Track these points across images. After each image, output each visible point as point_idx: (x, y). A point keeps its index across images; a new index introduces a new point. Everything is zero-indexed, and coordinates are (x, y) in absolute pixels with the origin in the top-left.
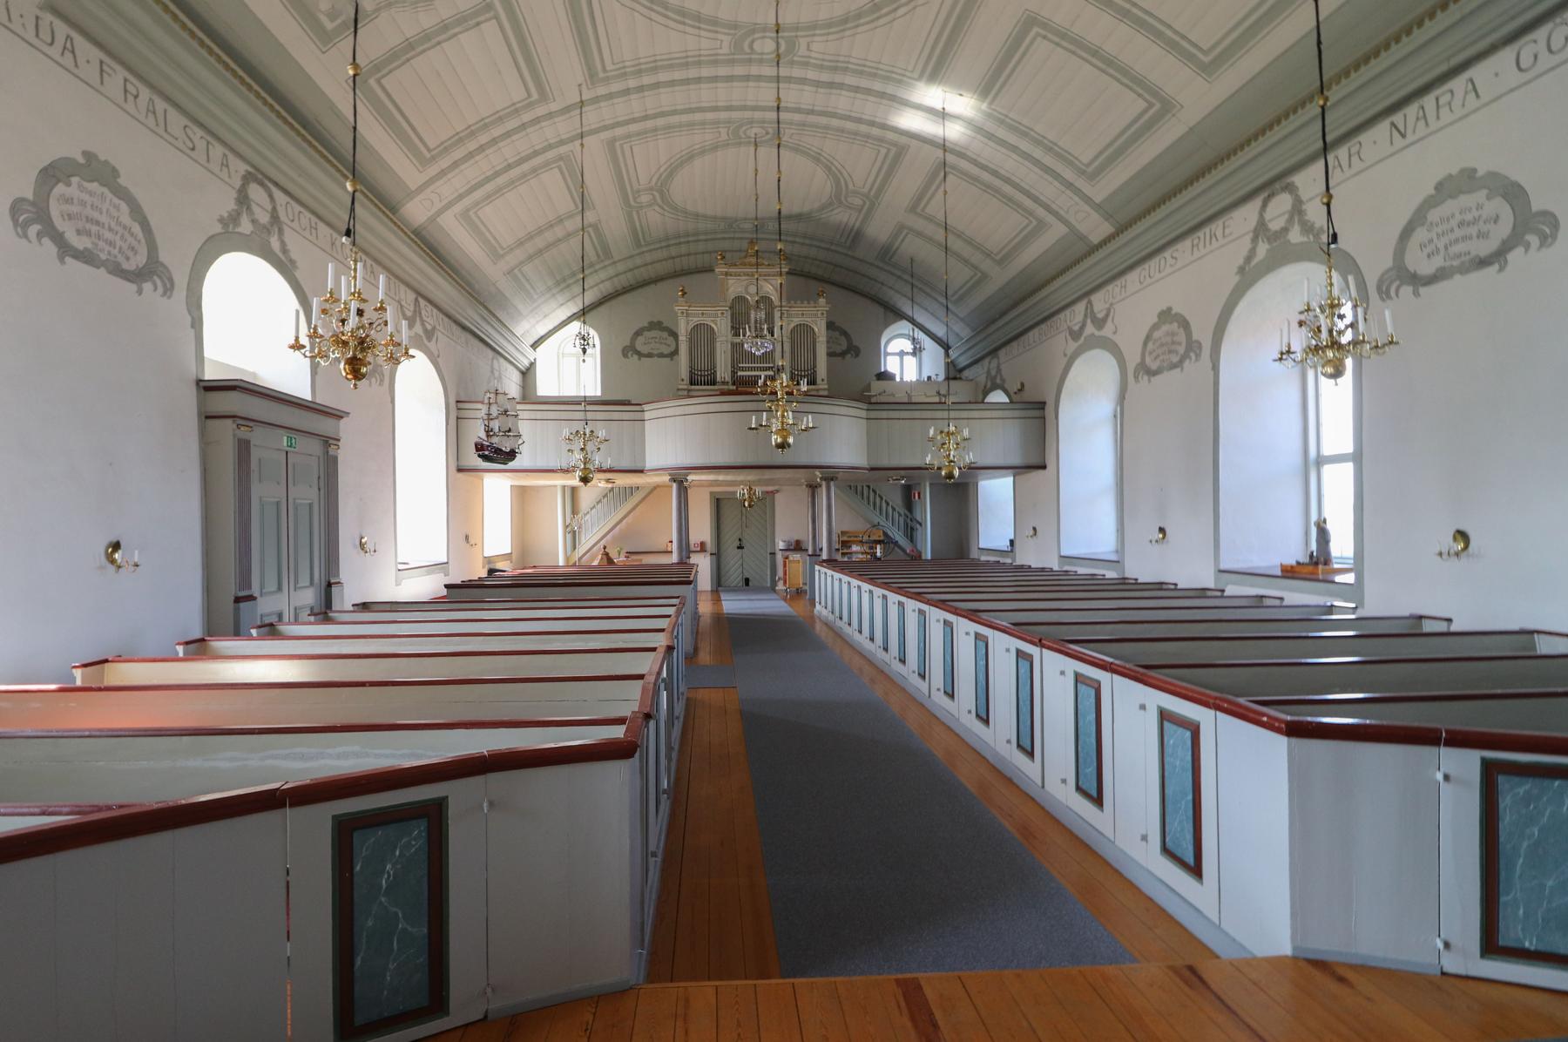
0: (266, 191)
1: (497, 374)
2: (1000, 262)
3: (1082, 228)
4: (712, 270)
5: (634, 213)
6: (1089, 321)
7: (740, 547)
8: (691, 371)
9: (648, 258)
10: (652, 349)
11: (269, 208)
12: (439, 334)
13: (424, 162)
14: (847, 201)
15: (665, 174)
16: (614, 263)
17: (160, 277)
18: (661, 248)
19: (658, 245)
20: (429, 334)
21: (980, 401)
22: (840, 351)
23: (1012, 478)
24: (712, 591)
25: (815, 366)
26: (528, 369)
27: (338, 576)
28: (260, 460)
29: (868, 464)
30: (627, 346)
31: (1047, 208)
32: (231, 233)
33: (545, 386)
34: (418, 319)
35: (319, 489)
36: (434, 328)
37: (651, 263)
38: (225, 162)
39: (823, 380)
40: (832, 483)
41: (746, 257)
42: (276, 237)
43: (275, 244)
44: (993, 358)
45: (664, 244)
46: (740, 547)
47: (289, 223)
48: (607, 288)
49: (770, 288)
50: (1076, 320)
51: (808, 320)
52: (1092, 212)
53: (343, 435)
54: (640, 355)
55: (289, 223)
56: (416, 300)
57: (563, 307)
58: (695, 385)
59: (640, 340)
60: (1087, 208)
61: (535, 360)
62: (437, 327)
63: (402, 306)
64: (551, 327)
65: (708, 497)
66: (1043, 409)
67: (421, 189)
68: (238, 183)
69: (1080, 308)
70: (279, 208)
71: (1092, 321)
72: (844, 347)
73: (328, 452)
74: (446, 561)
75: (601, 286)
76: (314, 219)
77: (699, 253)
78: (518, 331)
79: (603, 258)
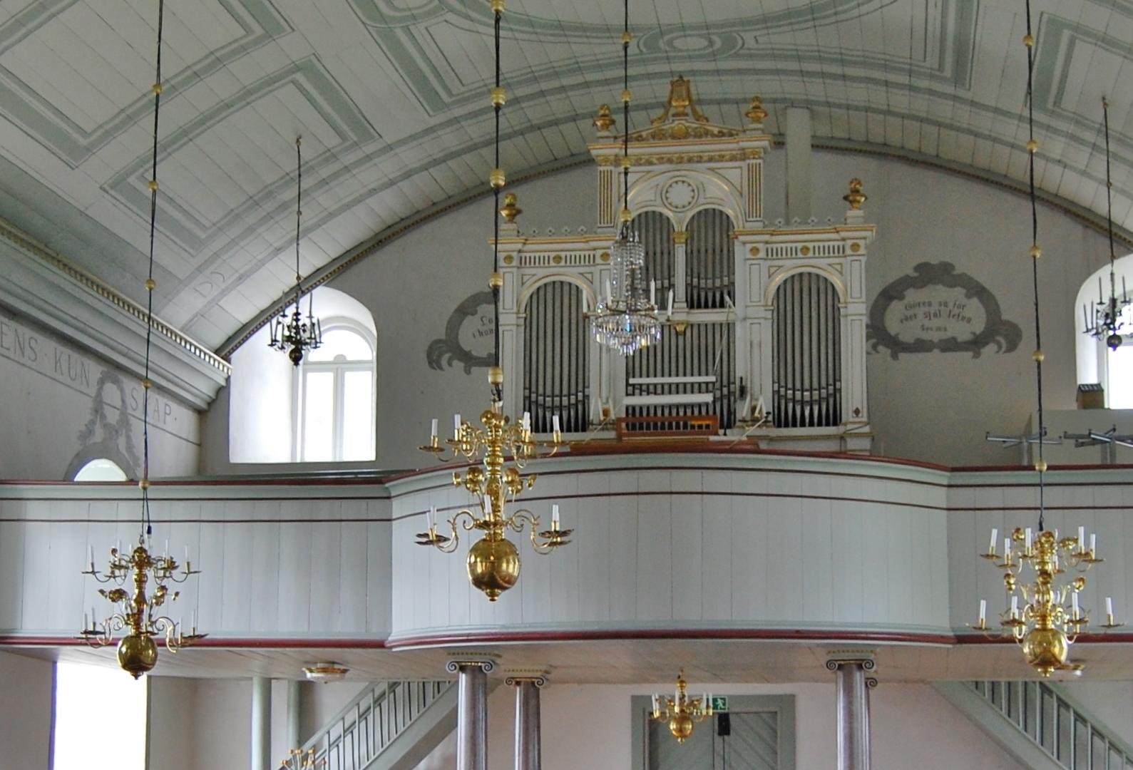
1: (113, 417)
5: (400, 34)
14: (396, 9)
16: (390, 147)
26: (211, 403)
30: (439, 341)
39: (857, 412)
41: (663, 119)
48: (387, 206)
51: (822, 266)
58: (786, 425)
59: (895, 311)
61: (228, 379)
65: (626, 706)
72: (979, 326)
75: (371, 201)
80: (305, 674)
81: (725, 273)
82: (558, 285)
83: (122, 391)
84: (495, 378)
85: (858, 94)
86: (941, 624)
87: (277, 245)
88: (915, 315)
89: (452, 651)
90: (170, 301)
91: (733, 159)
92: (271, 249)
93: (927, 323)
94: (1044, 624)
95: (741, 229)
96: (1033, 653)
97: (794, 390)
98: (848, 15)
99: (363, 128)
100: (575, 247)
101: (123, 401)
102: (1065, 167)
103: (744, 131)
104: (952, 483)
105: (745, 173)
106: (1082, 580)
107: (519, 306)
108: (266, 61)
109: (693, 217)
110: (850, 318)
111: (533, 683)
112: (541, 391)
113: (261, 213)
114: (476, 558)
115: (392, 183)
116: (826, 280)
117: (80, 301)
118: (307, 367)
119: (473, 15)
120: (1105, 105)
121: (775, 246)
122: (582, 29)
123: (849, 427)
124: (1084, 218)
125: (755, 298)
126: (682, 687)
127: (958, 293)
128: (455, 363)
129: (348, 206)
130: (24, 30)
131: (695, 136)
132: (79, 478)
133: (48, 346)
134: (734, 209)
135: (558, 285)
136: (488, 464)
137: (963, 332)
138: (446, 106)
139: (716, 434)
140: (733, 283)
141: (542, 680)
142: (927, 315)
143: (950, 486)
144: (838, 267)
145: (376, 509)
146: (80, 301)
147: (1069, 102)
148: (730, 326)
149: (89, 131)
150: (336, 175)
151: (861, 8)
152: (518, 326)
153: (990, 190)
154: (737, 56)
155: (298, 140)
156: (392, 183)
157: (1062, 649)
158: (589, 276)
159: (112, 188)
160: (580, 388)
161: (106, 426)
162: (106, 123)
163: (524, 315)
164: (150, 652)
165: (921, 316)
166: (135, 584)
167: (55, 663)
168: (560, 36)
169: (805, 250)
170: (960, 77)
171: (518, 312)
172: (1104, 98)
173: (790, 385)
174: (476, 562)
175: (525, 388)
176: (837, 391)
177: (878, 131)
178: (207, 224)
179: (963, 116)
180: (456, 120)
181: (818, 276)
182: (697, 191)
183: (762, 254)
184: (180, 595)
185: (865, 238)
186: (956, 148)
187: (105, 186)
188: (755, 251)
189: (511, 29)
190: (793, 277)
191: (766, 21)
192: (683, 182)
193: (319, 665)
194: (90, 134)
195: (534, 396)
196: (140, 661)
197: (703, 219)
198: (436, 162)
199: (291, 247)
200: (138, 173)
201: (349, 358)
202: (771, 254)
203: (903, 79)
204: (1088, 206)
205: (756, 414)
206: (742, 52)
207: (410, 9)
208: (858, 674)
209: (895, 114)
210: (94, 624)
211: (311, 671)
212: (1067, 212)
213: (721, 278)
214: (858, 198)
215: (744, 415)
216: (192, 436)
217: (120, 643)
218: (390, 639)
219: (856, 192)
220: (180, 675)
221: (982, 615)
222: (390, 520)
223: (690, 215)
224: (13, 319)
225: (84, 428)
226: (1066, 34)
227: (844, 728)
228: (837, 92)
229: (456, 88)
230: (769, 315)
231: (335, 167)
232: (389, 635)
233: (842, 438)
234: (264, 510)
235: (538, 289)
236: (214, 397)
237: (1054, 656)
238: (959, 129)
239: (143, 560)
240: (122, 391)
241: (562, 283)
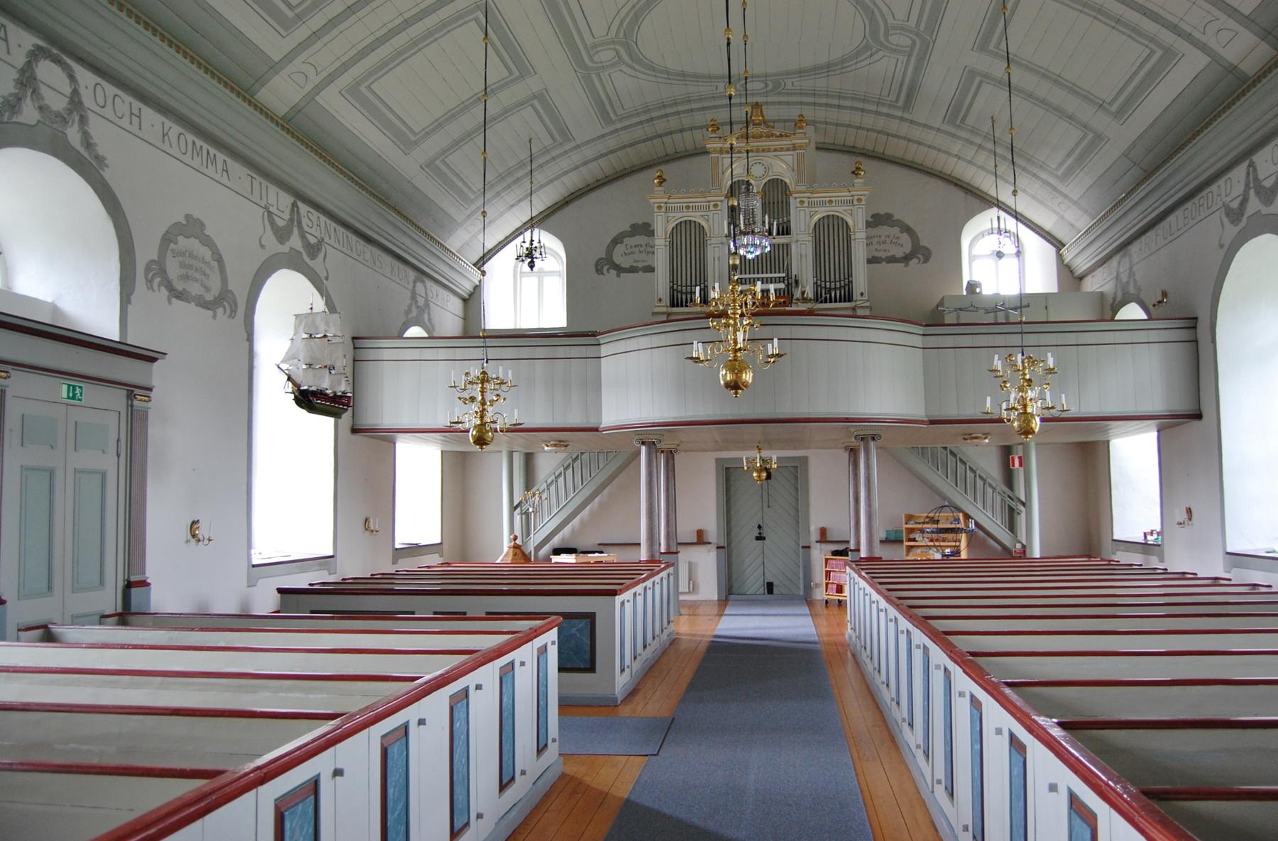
0: (63, 70)
1: (421, 302)
2: (1119, 114)
3: (1231, 54)
4: (705, 152)
6: (1252, 192)
7: (760, 538)
8: (672, 288)
9: (626, 137)
10: (635, 261)
11: (68, 90)
12: (328, 247)
13: (287, 25)
15: (627, 21)
16: (578, 146)
17: (228, 302)
18: (641, 123)
19: (637, 120)
20: (313, 250)
21: (1108, 316)
22: (903, 255)
23: (1155, 434)
24: (719, 600)
25: (850, 275)
26: (471, 295)
27: (144, 573)
28: (76, 422)
29: (927, 416)
30: (601, 259)
31: (1174, 28)
32: (7, 123)
33: (497, 317)
34: (296, 230)
35: (118, 456)
36: (321, 241)
37: (631, 145)
38: (225, 168)
39: (862, 294)
40: (872, 444)
42: (76, 126)
43: (73, 135)
44: (1124, 256)
45: (643, 118)
46: (760, 538)
47: (98, 110)
48: (572, 181)
49: (782, 167)
50: (1233, 195)
51: (840, 211)
52: (1241, 29)
53: (155, 382)
54: (620, 269)
55: (98, 110)
56: (294, 205)
57: (514, 209)
59: (620, 249)
60: (1232, 24)
62: (326, 239)
63: (270, 213)
64: (501, 237)
65: (711, 466)
66: (1195, 327)
67: (289, 58)
68: (21, 60)
69: (1239, 173)
70: (82, 90)
71: (1258, 193)
72: (908, 248)
73: (132, 406)
74: (331, 554)
75: (565, 179)
76: (137, 104)
77: (697, 128)
78: (454, 243)
79: (559, 139)
80: (544, 448)
81: (785, 215)
82: (688, 222)
83: (425, 287)
84: (734, 261)
85: (845, 117)
86: (919, 412)
87: (511, 203)
88: (872, 243)
89: (638, 433)
90: (451, 235)
91: (788, 150)
92: (508, 206)
93: (879, 247)
94: (1026, 410)
95: (793, 190)
96: (1020, 426)
97: (825, 282)
98: (849, 69)
99: (566, 135)
100: (699, 201)
101: (426, 293)
102: (959, 159)
103: (795, 134)
104: (925, 333)
105: (795, 158)
106: (1048, 384)
107: (666, 234)
108: (519, 91)
109: (765, 184)
110: (857, 241)
111: (671, 451)
112: (679, 284)
113: (505, 184)
114: (726, 371)
115: (577, 168)
116: (843, 219)
117: (405, 233)
118: (522, 275)
119: (636, 67)
120: (993, 121)
121: (813, 199)
122: (697, 77)
123: (858, 303)
124: (965, 188)
125: (803, 229)
126: (759, 452)
127: (896, 230)
128: (611, 271)
129: (551, 181)
130: (387, 69)
131: (766, 137)
132: (406, 335)
133: (388, 259)
134: (789, 178)
135: (688, 222)
136: (732, 314)
137: (899, 253)
138: (613, 122)
139: (788, 306)
140: (790, 221)
141: (676, 450)
142: (879, 243)
143: (924, 335)
144: (849, 212)
145: (591, 351)
146: (405, 233)
147: (970, 121)
148: (788, 246)
149: (417, 132)
150: (547, 162)
151: (858, 64)
152: (666, 246)
153: (914, 173)
154: (779, 94)
155: (530, 141)
156: (577, 168)
157: (1036, 424)
158: (706, 217)
159: (427, 166)
160: (702, 282)
161: (418, 307)
162: (427, 127)
163: (669, 240)
164: (490, 434)
165: (875, 243)
166: (480, 393)
167: (395, 444)
168: (682, 80)
169: (831, 202)
170: (907, 105)
171: (666, 238)
172: (992, 118)
173: (823, 280)
174: (726, 374)
175: (670, 282)
176: (850, 282)
177: (851, 139)
178: (475, 190)
179: (905, 129)
180: (617, 131)
181: (838, 217)
182: (767, 169)
183: (806, 204)
184: (506, 400)
185: (865, 195)
186: (896, 149)
187: (423, 166)
188: (802, 202)
189: (656, 76)
190: (824, 217)
191: (801, 73)
192: (760, 163)
193: (552, 443)
194: (418, 134)
195: (675, 286)
196: (484, 439)
197: (771, 184)
198: (602, 156)
199: (527, 200)
200: (441, 159)
201: (546, 270)
202: (811, 204)
203: (873, 108)
204: (968, 182)
205: (805, 296)
206: (784, 91)
207: (601, 62)
208: (872, 443)
209: (863, 129)
210: (458, 417)
211: (547, 446)
212: (956, 185)
213: (783, 218)
214: (860, 172)
215: (798, 296)
216: (461, 314)
217: (471, 430)
218: (602, 426)
219: (858, 169)
220: (459, 450)
221: (988, 405)
222: (600, 358)
223: (764, 182)
224: (369, 244)
225: (406, 309)
226: (978, 79)
227: (865, 474)
228: (833, 115)
229: (620, 111)
230: (810, 239)
231: (548, 157)
232: (601, 424)
233: (854, 309)
234: (525, 353)
235: (677, 225)
236: (472, 291)
237: (1032, 428)
238: (899, 137)
239: (484, 379)
240: (425, 287)
241: (690, 221)
